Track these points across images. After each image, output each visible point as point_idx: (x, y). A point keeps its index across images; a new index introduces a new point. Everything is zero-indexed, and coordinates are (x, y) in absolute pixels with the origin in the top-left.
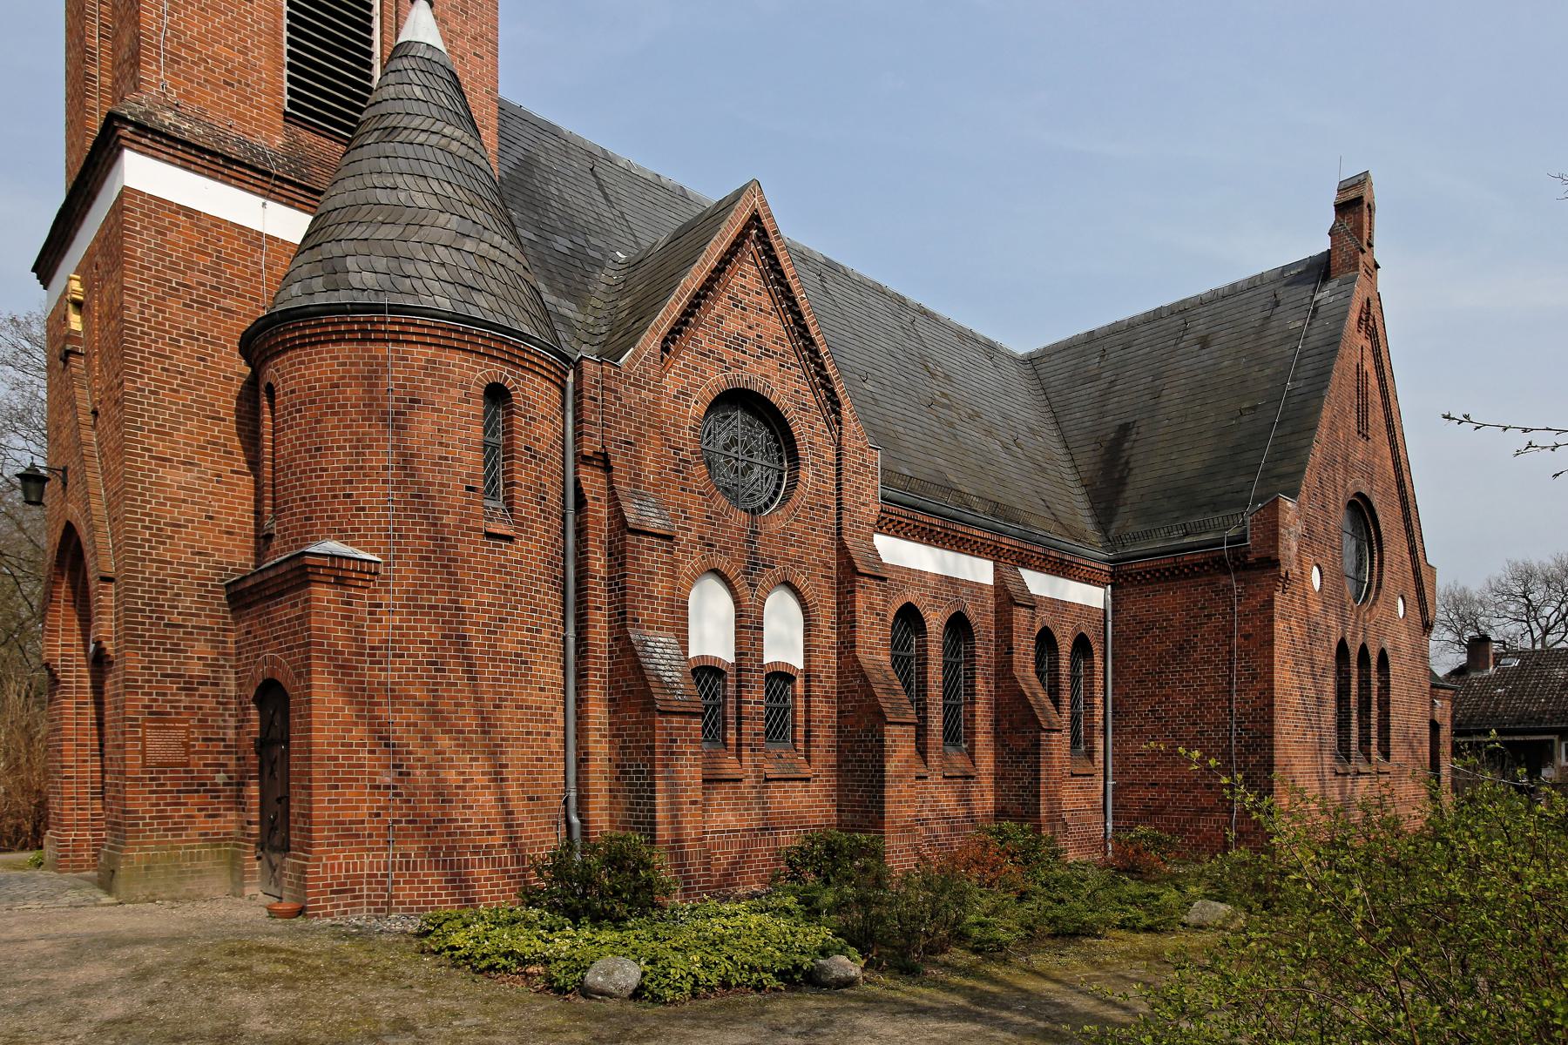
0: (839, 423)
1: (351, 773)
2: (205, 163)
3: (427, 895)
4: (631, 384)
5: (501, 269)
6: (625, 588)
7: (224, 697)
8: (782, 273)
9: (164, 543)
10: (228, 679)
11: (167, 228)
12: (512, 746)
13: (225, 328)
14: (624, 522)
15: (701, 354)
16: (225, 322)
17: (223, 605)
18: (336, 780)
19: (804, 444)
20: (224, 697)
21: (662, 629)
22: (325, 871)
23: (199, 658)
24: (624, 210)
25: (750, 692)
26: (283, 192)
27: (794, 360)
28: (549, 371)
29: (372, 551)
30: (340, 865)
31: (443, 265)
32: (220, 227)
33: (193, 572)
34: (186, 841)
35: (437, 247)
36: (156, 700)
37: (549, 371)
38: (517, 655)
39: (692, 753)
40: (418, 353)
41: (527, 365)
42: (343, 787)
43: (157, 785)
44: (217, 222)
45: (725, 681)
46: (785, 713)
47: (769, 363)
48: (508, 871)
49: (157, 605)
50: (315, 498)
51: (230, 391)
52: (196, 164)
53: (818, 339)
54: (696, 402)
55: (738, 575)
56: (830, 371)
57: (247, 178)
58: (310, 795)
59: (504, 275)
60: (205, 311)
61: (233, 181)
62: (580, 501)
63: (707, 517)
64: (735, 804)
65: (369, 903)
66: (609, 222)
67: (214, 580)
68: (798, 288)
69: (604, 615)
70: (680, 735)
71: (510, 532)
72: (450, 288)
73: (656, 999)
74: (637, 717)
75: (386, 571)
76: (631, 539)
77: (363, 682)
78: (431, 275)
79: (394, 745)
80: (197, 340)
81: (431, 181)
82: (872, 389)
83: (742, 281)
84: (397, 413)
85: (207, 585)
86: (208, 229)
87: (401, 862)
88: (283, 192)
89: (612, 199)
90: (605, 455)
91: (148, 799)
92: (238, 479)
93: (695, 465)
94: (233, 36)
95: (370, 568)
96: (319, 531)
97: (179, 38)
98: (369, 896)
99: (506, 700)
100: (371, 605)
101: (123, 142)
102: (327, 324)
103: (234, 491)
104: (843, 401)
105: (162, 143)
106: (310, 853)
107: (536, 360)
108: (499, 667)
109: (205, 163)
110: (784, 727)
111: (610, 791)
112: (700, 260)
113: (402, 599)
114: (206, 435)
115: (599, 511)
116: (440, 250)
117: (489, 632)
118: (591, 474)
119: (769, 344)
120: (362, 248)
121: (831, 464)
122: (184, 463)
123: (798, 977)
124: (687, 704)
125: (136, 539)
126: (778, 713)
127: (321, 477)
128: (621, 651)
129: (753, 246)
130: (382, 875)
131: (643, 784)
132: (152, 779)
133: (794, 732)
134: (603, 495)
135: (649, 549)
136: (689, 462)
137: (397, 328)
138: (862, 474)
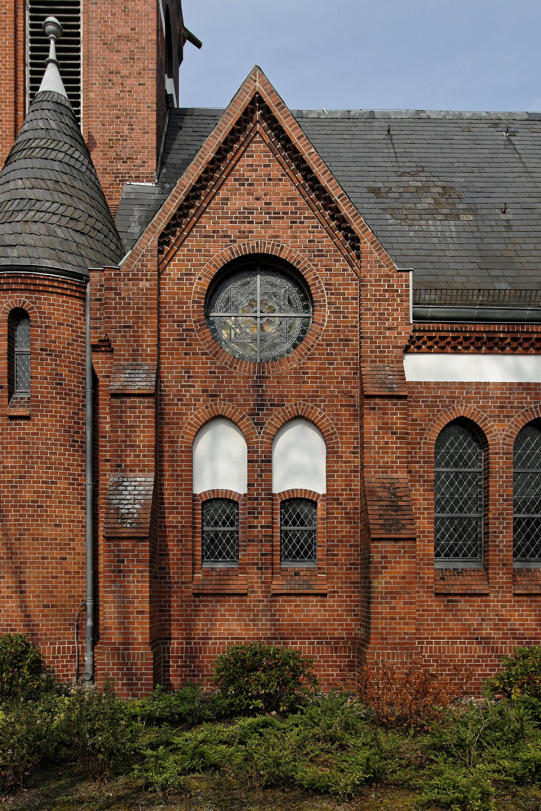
12: (30, 568)
15: (205, 236)
21: (143, 471)
38: (33, 501)
39: (139, 571)
41: (41, 288)
54: (200, 279)
55: (244, 417)
56: (345, 211)
63: (211, 372)
64: (239, 615)
93: (198, 331)
99: (25, 535)
107: (47, 283)
108: (19, 511)
117: (12, 487)
118: (102, 359)
119: (279, 207)
135: (131, 407)
136: (192, 330)
138: (388, 300)
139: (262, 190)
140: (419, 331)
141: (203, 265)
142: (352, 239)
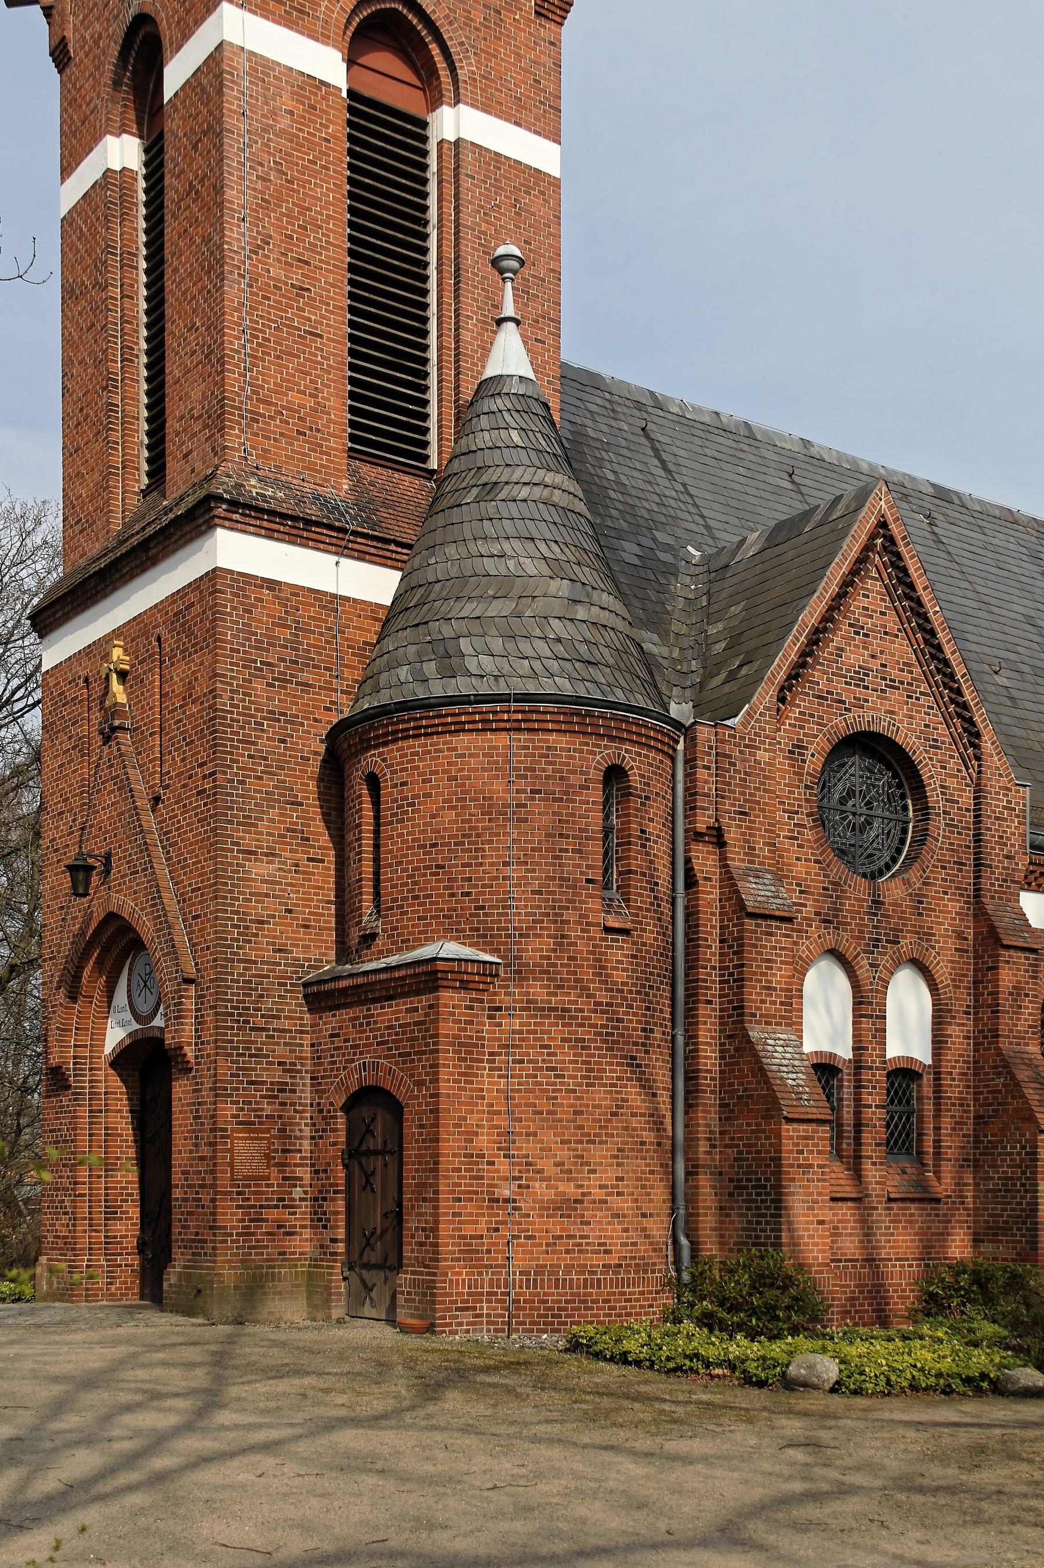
0: (978, 758)
1: (472, 1185)
2: (287, 529)
3: (547, 1316)
4: (746, 746)
5: (612, 633)
6: (742, 979)
7: (300, 1104)
8: (912, 586)
9: (250, 942)
10: (304, 1085)
11: (252, 605)
13: (303, 704)
14: (741, 904)
16: (302, 698)
17: (301, 1005)
18: (459, 1192)
19: (935, 789)
20: (300, 1104)
22: (451, 1288)
23: (280, 1064)
24: (687, 480)
25: (870, 1094)
26: (356, 546)
27: (924, 687)
28: (663, 743)
29: (492, 952)
30: (464, 1281)
31: (559, 640)
32: (298, 595)
33: (274, 971)
34: (267, 1260)
35: (551, 621)
36: (242, 1109)
37: (663, 743)
40: (539, 740)
42: (465, 1200)
43: (244, 1200)
44: (296, 590)
45: (842, 1080)
46: (908, 1119)
47: (895, 696)
48: (624, 1294)
49: (244, 1008)
50: (430, 896)
51: (306, 772)
52: (279, 531)
53: (953, 659)
54: (813, 755)
56: (968, 696)
57: (323, 538)
58: (436, 1208)
59: (615, 639)
60: (285, 688)
61: (311, 543)
62: (691, 881)
65: (488, 1323)
66: (673, 503)
67: (291, 978)
68: (930, 601)
69: (715, 1010)
70: (807, 1146)
71: (628, 925)
72: (568, 666)
73: (857, 1392)
74: (758, 1125)
75: (506, 972)
76: (750, 924)
77: (482, 1090)
78: (549, 654)
79: (513, 1156)
80: (279, 720)
81: (538, 543)
82: (1006, 682)
83: (865, 602)
84: (518, 806)
85: (285, 984)
86: (288, 600)
87: (521, 1280)
88: (356, 546)
89: (671, 467)
90: (719, 829)
91: (235, 1214)
92: (314, 867)
94: (305, 380)
95: (491, 970)
96: (433, 931)
97: (258, 393)
98: (489, 1315)
100: (490, 1009)
101: (217, 521)
102: (446, 716)
103: (309, 880)
104: (983, 732)
105: (250, 516)
106: (437, 1267)
109: (287, 529)
110: (908, 1135)
111: (721, 1208)
112: (820, 589)
113: (522, 1001)
114: (285, 822)
115: (710, 894)
116: (554, 623)
119: (894, 673)
120: (476, 629)
121: (968, 810)
122: (266, 855)
123: (985, 1385)
124: (815, 1110)
125: (226, 939)
126: (900, 1118)
127: (438, 874)
128: (736, 1050)
129: (877, 558)
130: (502, 1294)
131: (766, 1201)
132: (239, 1193)
133: (920, 1141)
134: (715, 873)
137: (520, 716)
138: (1005, 820)
139: (878, 645)
140: (1035, 864)
141: (816, 736)
142: (970, 733)
